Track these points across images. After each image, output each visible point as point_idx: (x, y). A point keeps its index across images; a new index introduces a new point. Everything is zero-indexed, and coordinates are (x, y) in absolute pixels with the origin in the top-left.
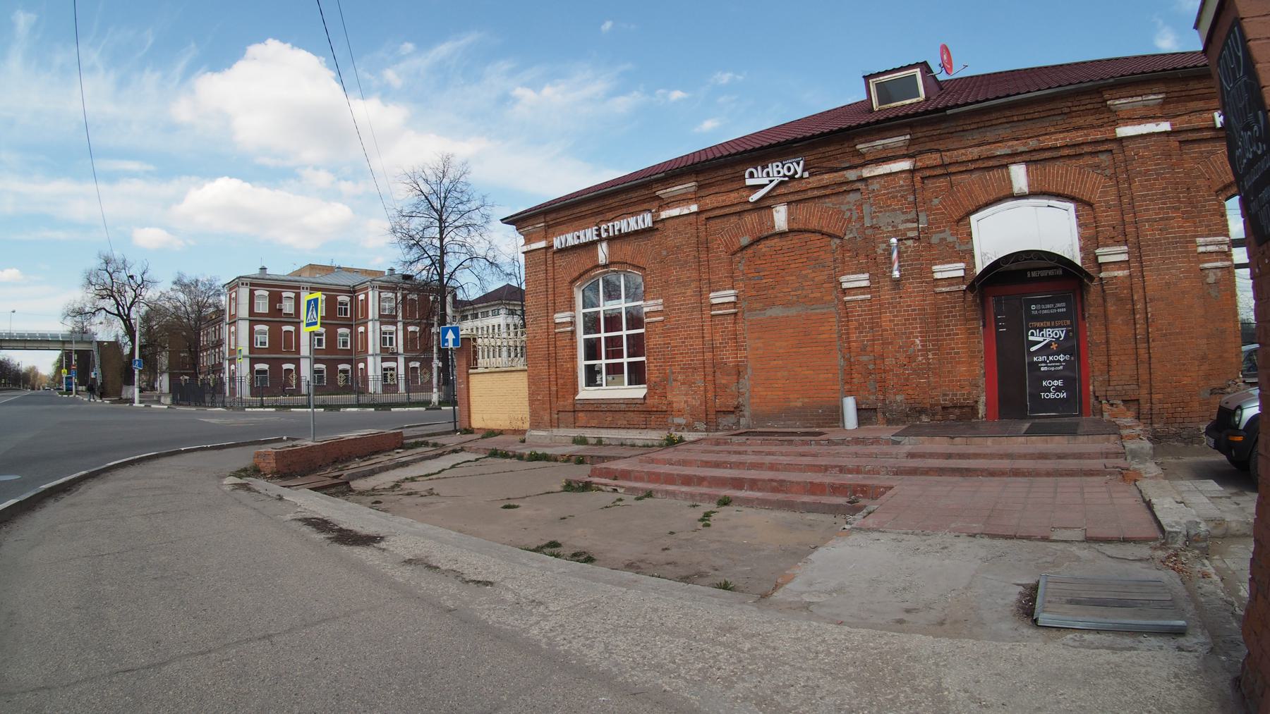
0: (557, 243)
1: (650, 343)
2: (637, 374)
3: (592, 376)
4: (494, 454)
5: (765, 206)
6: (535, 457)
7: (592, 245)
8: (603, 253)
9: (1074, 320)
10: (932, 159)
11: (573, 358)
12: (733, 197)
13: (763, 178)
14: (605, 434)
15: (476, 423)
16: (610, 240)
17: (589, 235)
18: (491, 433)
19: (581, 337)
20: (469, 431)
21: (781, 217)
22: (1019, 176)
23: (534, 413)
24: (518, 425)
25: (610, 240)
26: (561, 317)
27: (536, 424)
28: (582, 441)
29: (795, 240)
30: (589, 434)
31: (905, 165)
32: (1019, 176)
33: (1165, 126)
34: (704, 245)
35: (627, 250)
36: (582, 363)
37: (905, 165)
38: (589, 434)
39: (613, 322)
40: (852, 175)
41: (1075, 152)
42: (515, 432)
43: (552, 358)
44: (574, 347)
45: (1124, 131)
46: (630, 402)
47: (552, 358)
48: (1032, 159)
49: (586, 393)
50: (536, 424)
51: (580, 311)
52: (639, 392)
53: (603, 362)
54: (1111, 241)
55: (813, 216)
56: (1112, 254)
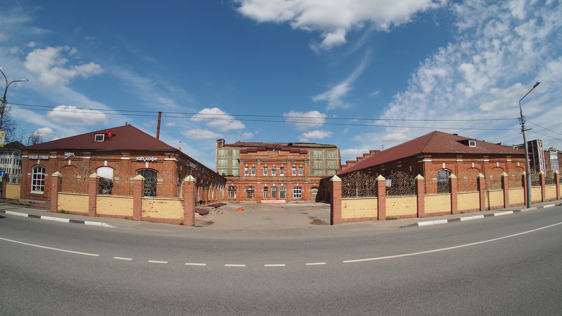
0: (30, 157)
1: (45, 183)
2: (43, 189)
3: (34, 188)
4: (12, 203)
5: (67, 160)
6: (21, 204)
7: (37, 160)
8: (39, 162)
9: (513, 39)
10: (93, 157)
11: (31, 184)
12: (62, 156)
13: (68, 154)
14: (35, 201)
15: (6, 197)
16: (40, 160)
17: (36, 157)
18: (10, 200)
19: (33, 179)
20: (5, 199)
21: (70, 162)
22: (106, 163)
23: (21, 195)
24: (17, 198)
25: (40, 160)
26: (29, 174)
27: (21, 198)
28: (30, 202)
29: (71, 167)
30: (32, 201)
31: (89, 158)
32: (106, 163)
33: (129, 158)
34: (56, 165)
35: (43, 162)
36: (32, 185)
37: (89, 158)
38: (32, 201)
39: (39, 176)
40: (81, 157)
41: (115, 160)
42: (16, 200)
43: (26, 183)
44: (31, 181)
45: (122, 158)
46: (41, 195)
47: (26, 183)
48: (109, 161)
49: (32, 192)
50: (21, 198)
51: (33, 173)
52: (42, 193)
53: (36, 185)
54: (42, 198)
55: (75, 163)
56: (116, 179)
